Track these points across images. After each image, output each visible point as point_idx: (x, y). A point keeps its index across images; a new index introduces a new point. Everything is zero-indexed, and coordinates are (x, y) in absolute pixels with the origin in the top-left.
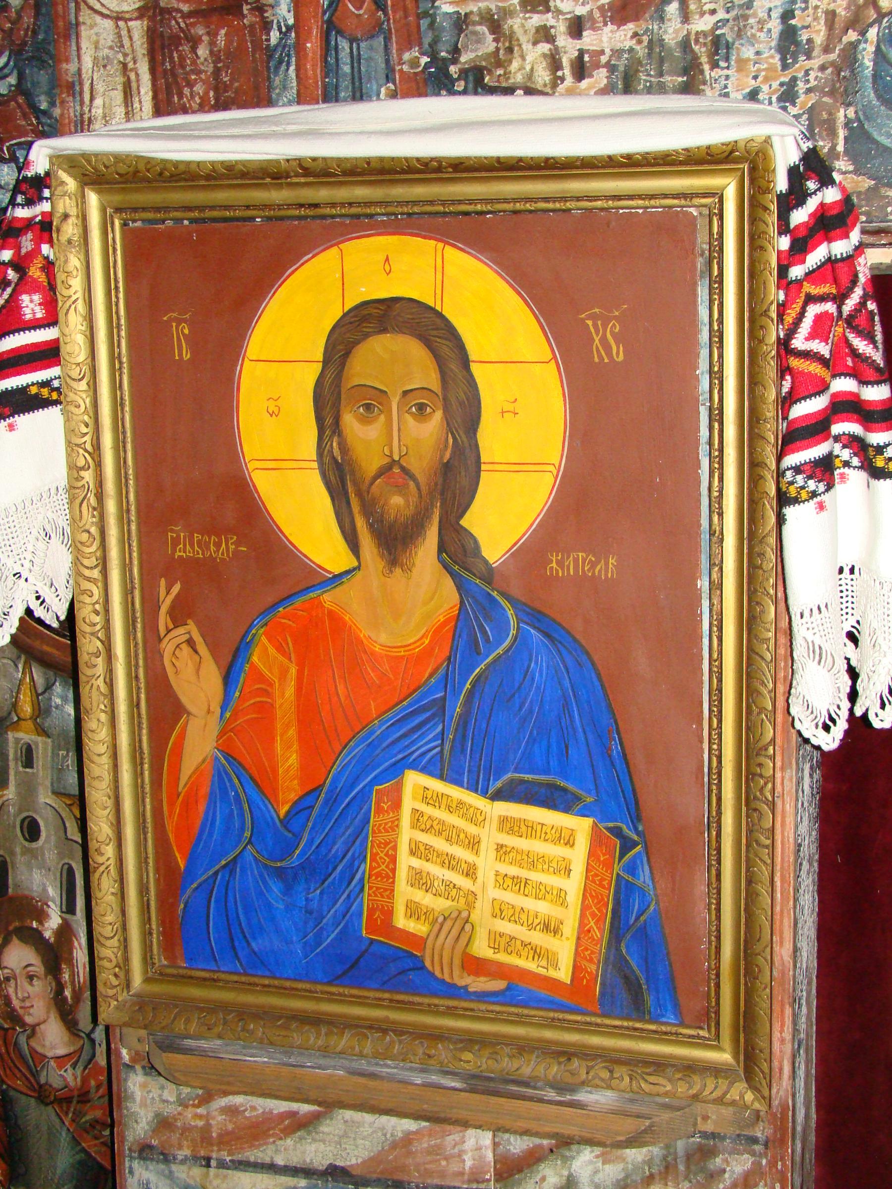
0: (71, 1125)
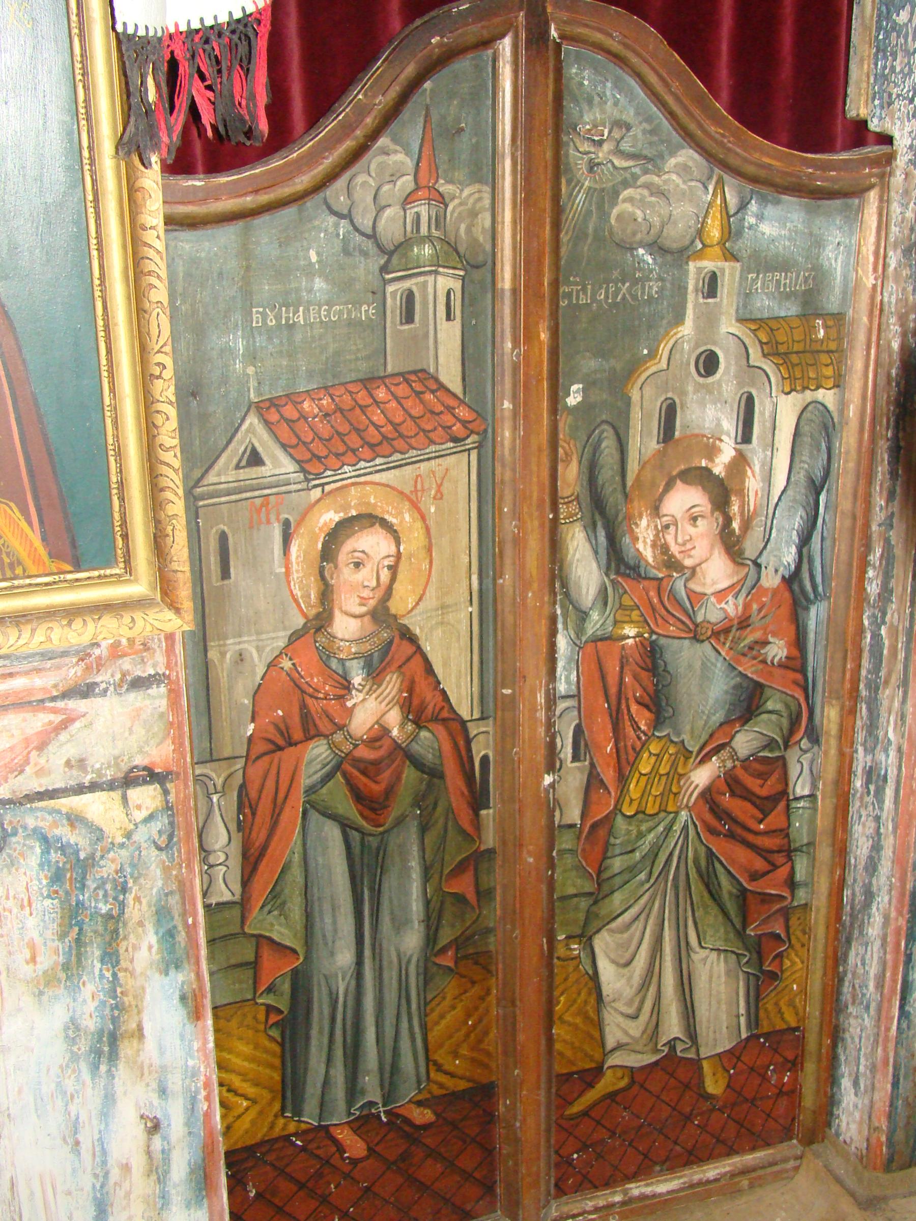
0: (727, 654)
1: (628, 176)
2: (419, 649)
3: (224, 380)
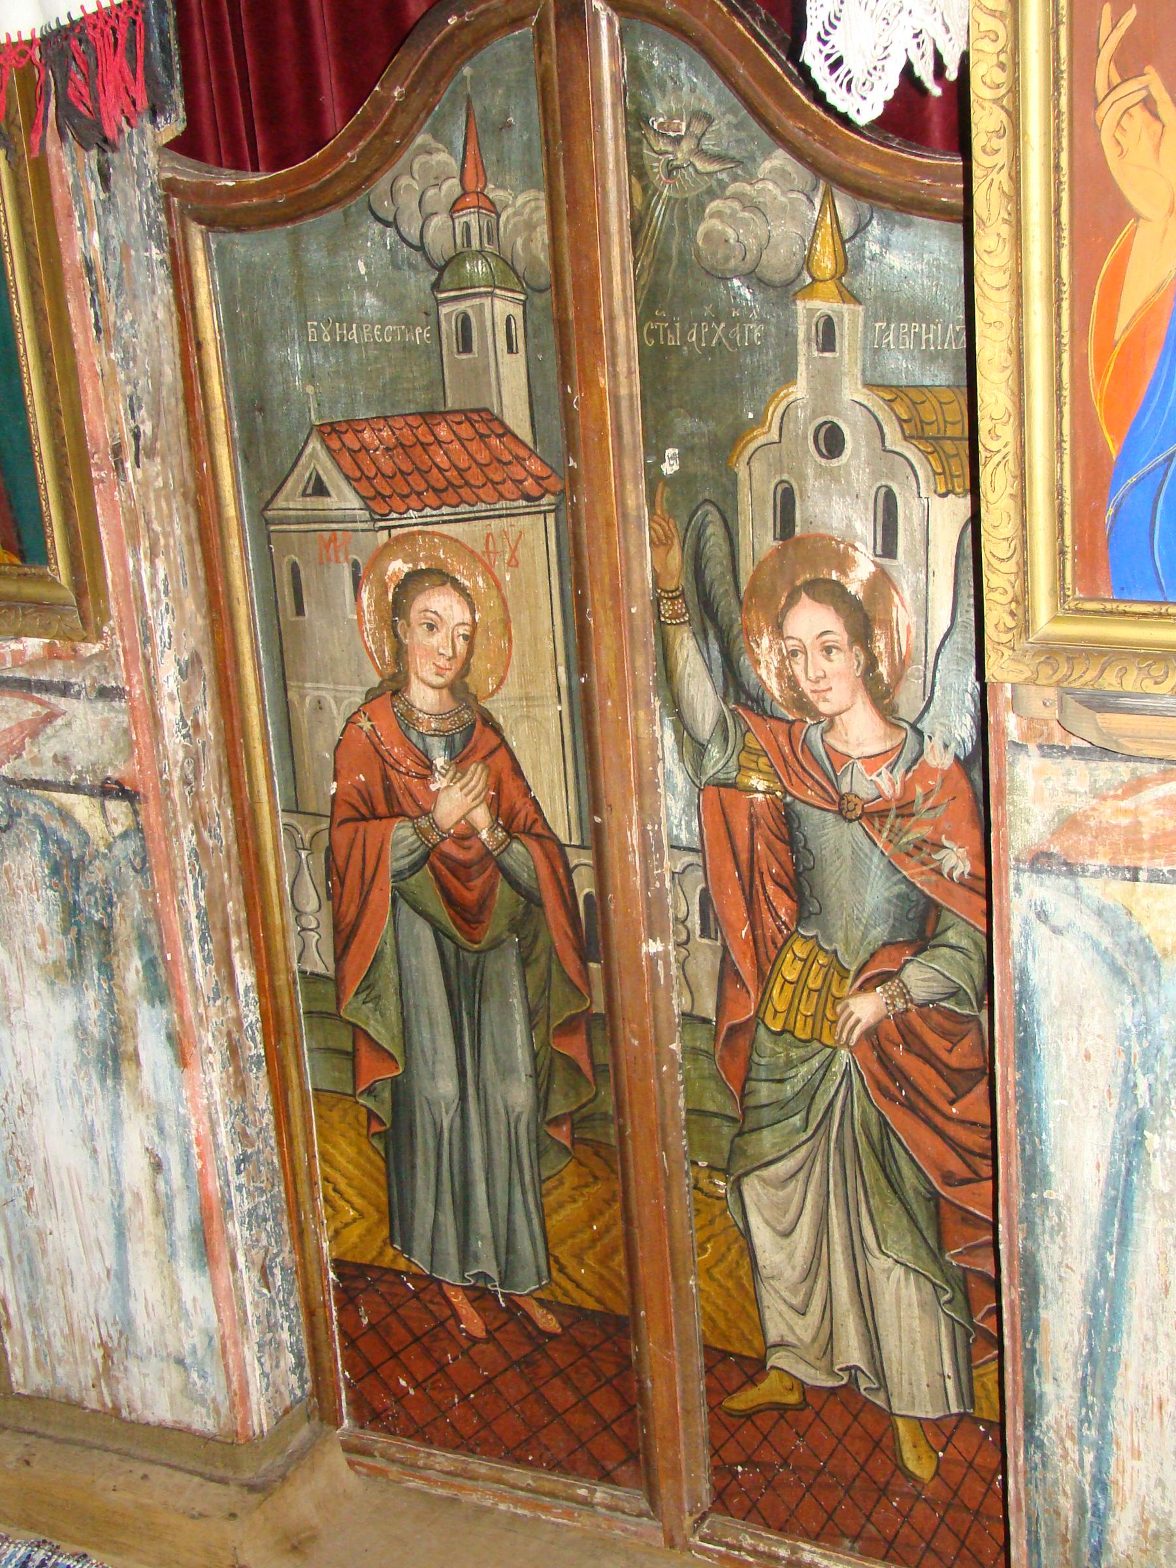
0: (886, 847)
1: (714, 183)
2: (504, 743)
3: (286, 399)
